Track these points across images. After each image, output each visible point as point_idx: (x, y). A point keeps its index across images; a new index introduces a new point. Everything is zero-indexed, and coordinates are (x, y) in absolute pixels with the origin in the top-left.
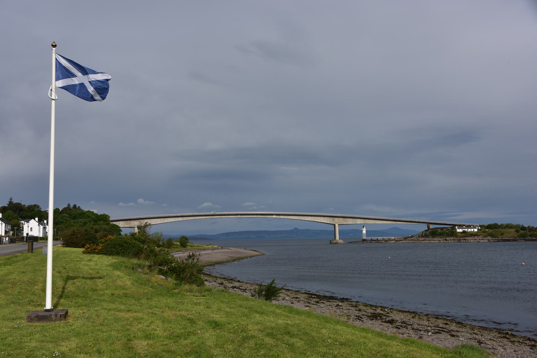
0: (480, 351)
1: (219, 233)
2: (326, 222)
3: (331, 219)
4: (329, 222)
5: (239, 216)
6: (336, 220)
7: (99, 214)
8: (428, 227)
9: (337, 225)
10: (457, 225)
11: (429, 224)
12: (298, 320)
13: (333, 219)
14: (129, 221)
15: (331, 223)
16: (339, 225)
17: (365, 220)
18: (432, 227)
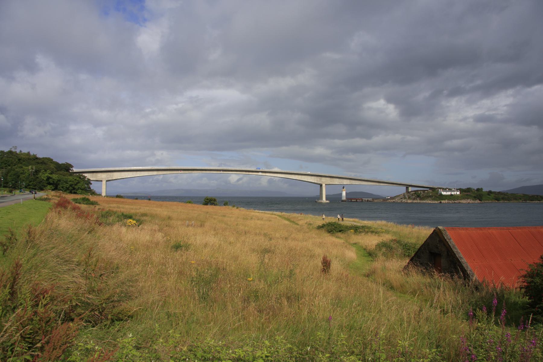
0: (271, 239)
1: (431, 233)
2: (313, 182)
3: (318, 178)
4: (316, 182)
5: (222, 172)
6: (324, 179)
7: (60, 163)
8: (408, 192)
9: (324, 185)
10: (440, 188)
11: (407, 186)
12: (196, 320)
13: (320, 179)
14: (95, 174)
15: (318, 182)
16: (326, 185)
17: (351, 181)
18: (410, 189)
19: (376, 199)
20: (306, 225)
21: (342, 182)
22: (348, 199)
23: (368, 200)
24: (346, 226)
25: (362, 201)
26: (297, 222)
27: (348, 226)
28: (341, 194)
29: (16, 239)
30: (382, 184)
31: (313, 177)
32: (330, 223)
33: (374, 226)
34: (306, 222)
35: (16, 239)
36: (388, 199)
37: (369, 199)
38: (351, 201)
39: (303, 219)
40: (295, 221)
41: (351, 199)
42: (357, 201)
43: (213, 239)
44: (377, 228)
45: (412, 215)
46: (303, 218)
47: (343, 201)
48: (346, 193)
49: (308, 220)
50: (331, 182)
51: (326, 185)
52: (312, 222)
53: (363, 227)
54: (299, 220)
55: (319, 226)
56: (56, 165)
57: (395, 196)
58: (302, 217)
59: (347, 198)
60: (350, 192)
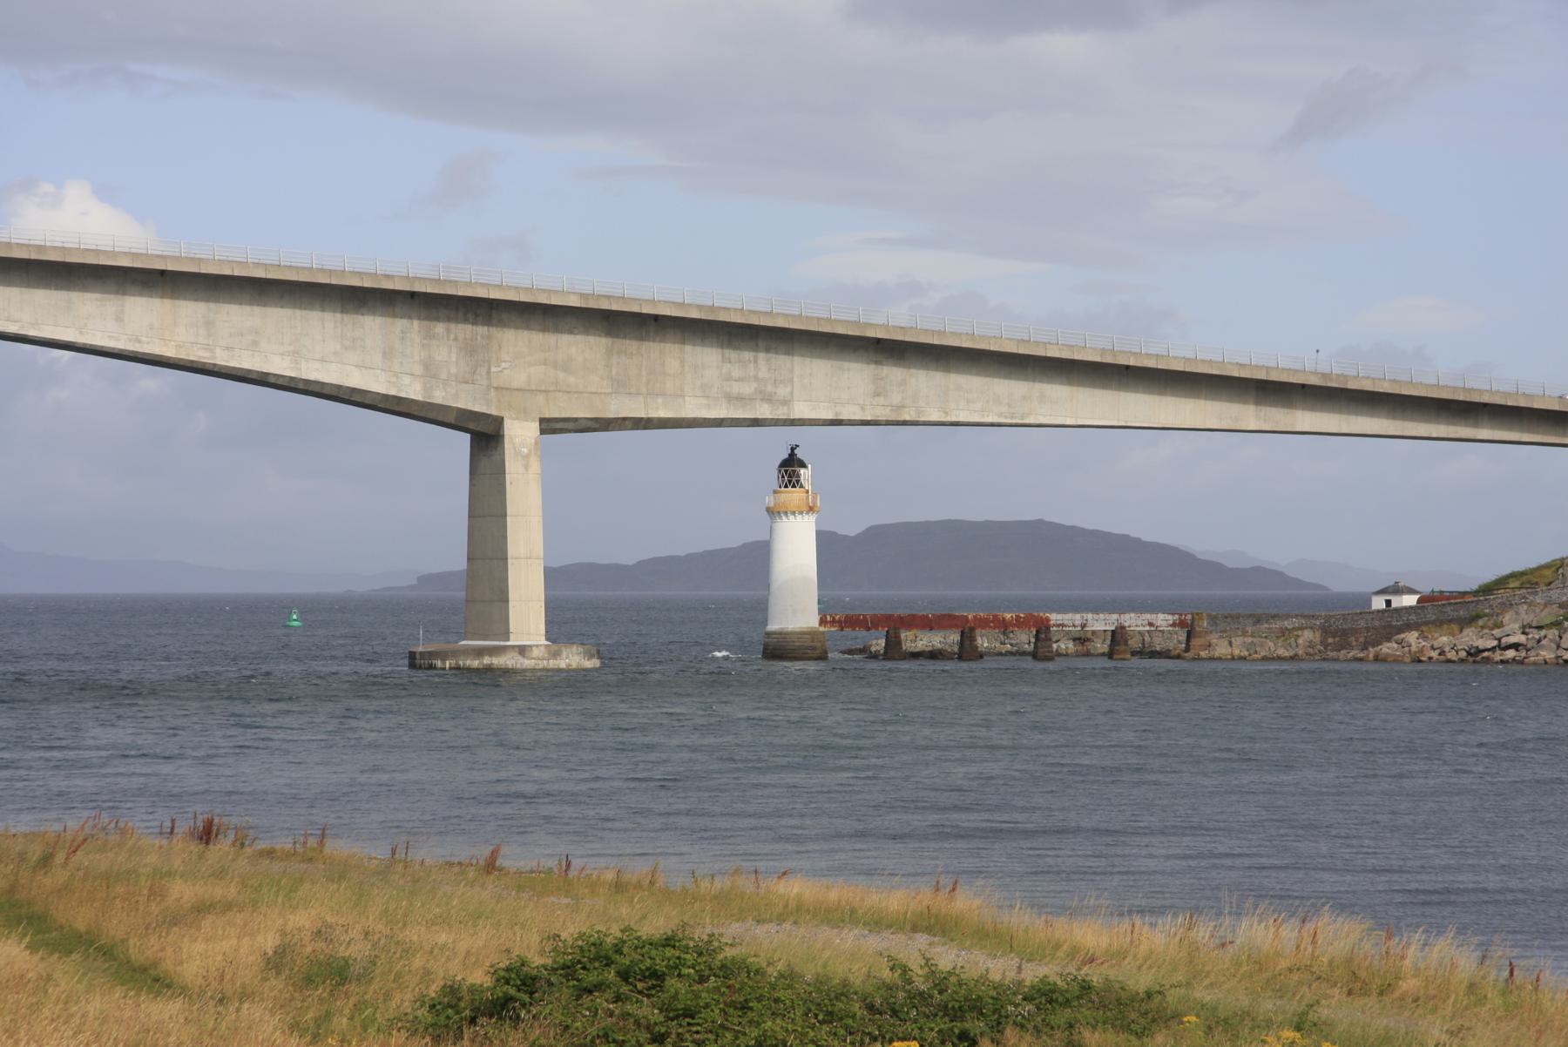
2: (377, 384)
4: (412, 390)
9: (520, 434)
13: (470, 350)
15: (439, 397)
16: (549, 426)
17: (893, 373)
19: (1231, 618)
20: (277, 984)
21: (768, 399)
22: (851, 622)
23: (1118, 636)
24: (820, 982)
25: (1041, 651)
26: (141, 949)
27: (844, 992)
28: (759, 556)
29: (394, 853)
30: (1305, 419)
31: (372, 326)
32: (598, 954)
33: (1201, 994)
34: (269, 942)
35: (394, 853)
36: (1392, 624)
37: (1134, 622)
38: (893, 650)
39: (228, 907)
40: (116, 926)
41: (894, 625)
42: (967, 651)
43: (227, 848)
44: (1246, 1014)
45: (866, 861)
46: (232, 892)
47: (779, 649)
48: (827, 542)
49: (302, 920)
50: (620, 386)
51: (549, 426)
52: (355, 950)
53: (1047, 997)
54: (175, 919)
55: (452, 990)
56: (381, 919)
57: (1489, 576)
58: (220, 874)
59: (840, 618)
60: (876, 534)
